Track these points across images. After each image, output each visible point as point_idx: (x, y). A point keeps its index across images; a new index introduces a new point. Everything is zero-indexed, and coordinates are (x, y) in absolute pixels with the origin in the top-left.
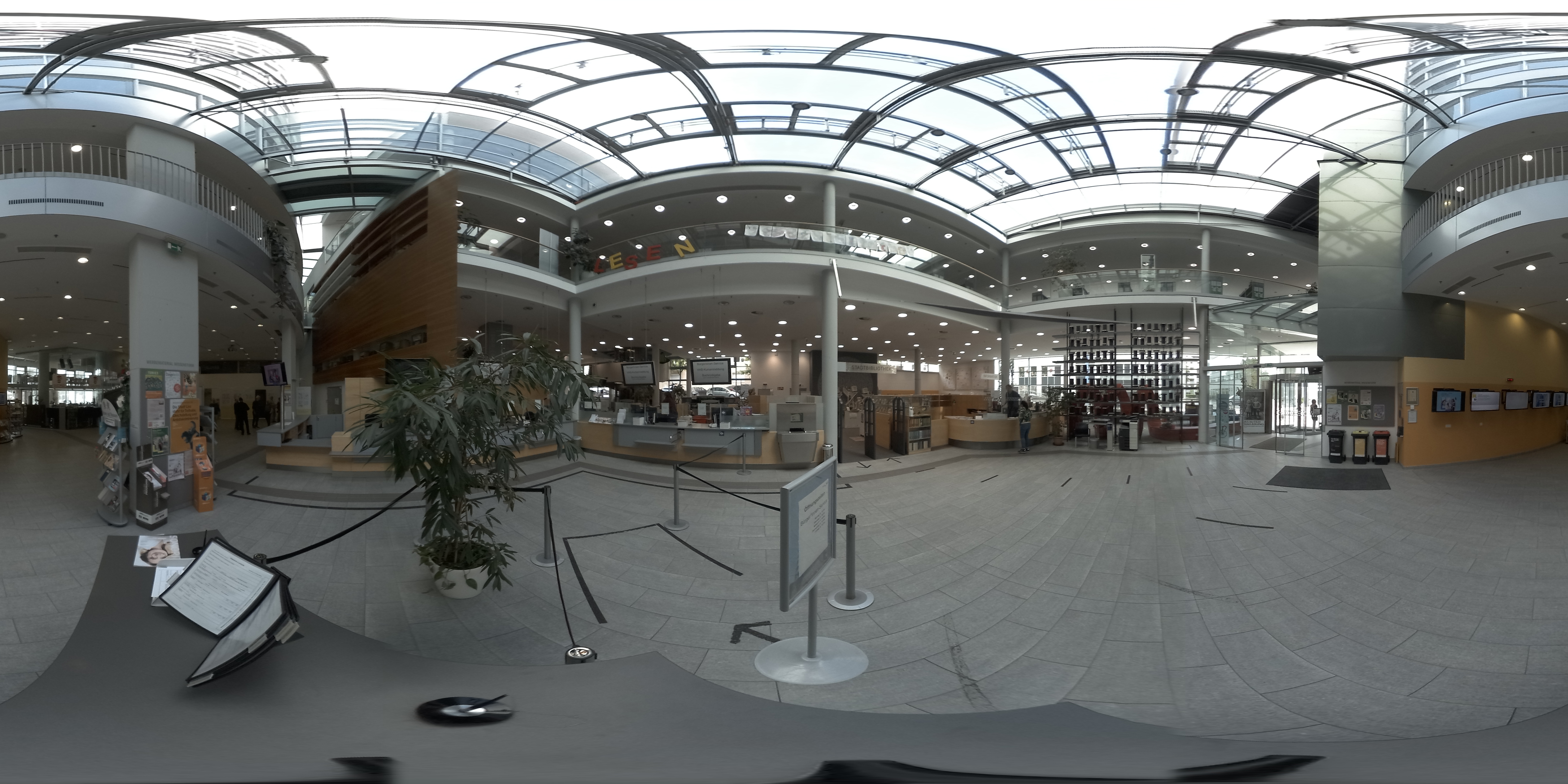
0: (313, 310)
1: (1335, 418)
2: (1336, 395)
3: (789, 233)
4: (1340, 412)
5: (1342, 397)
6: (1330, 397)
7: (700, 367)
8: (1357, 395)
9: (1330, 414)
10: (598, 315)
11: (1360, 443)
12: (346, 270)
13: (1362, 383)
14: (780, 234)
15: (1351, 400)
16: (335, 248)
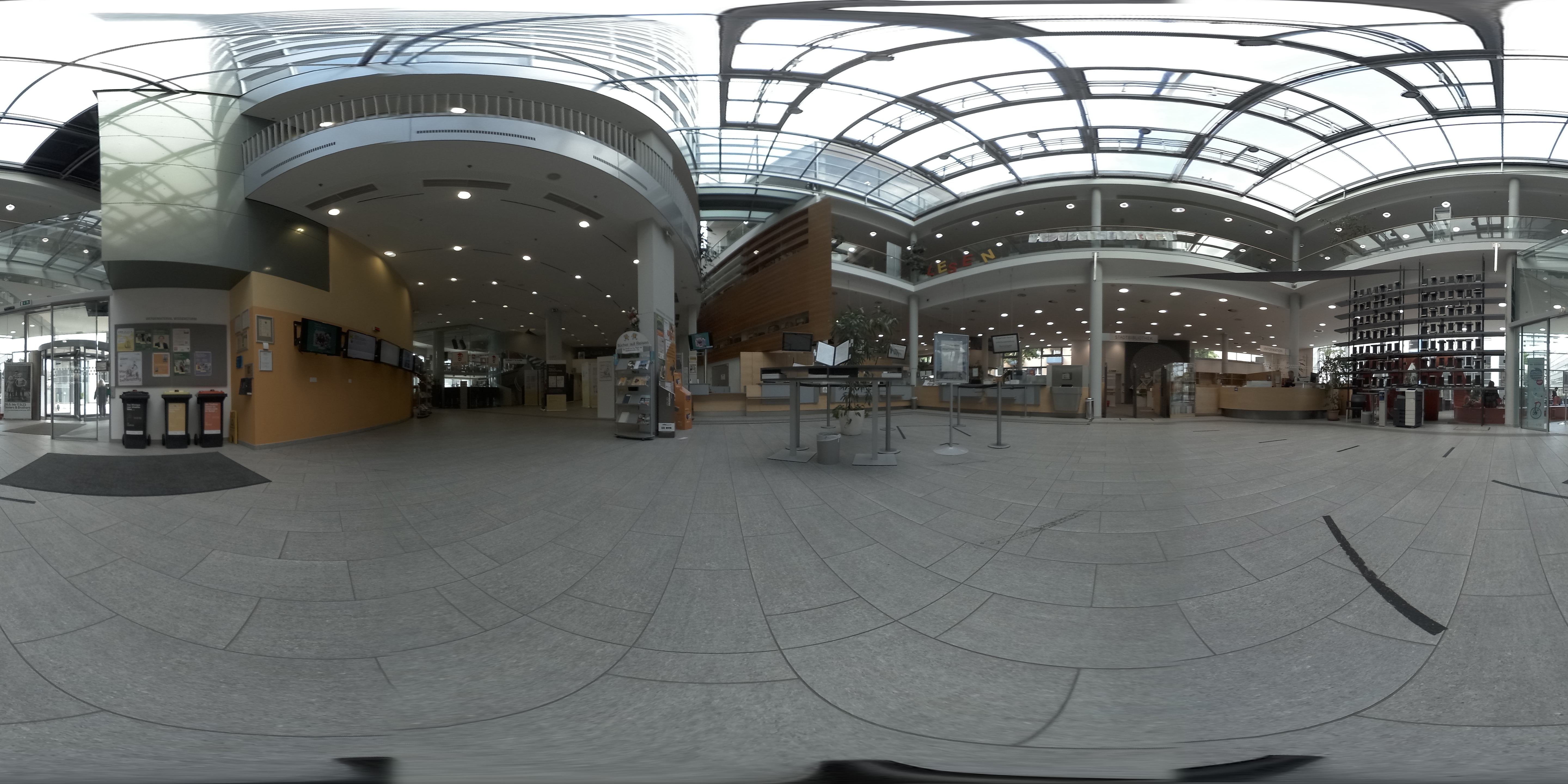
1: (131, 375)
2: (132, 338)
3: (1061, 237)
4: (139, 364)
5: (143, 340)
6: (122, 341)
8: (167, 337)
9: (124, 366)
10: (931, 308)
11: (176, 410)
12: (721, 278)
13: (175, 319)
14: (1054, 238)
15: (158, 345)
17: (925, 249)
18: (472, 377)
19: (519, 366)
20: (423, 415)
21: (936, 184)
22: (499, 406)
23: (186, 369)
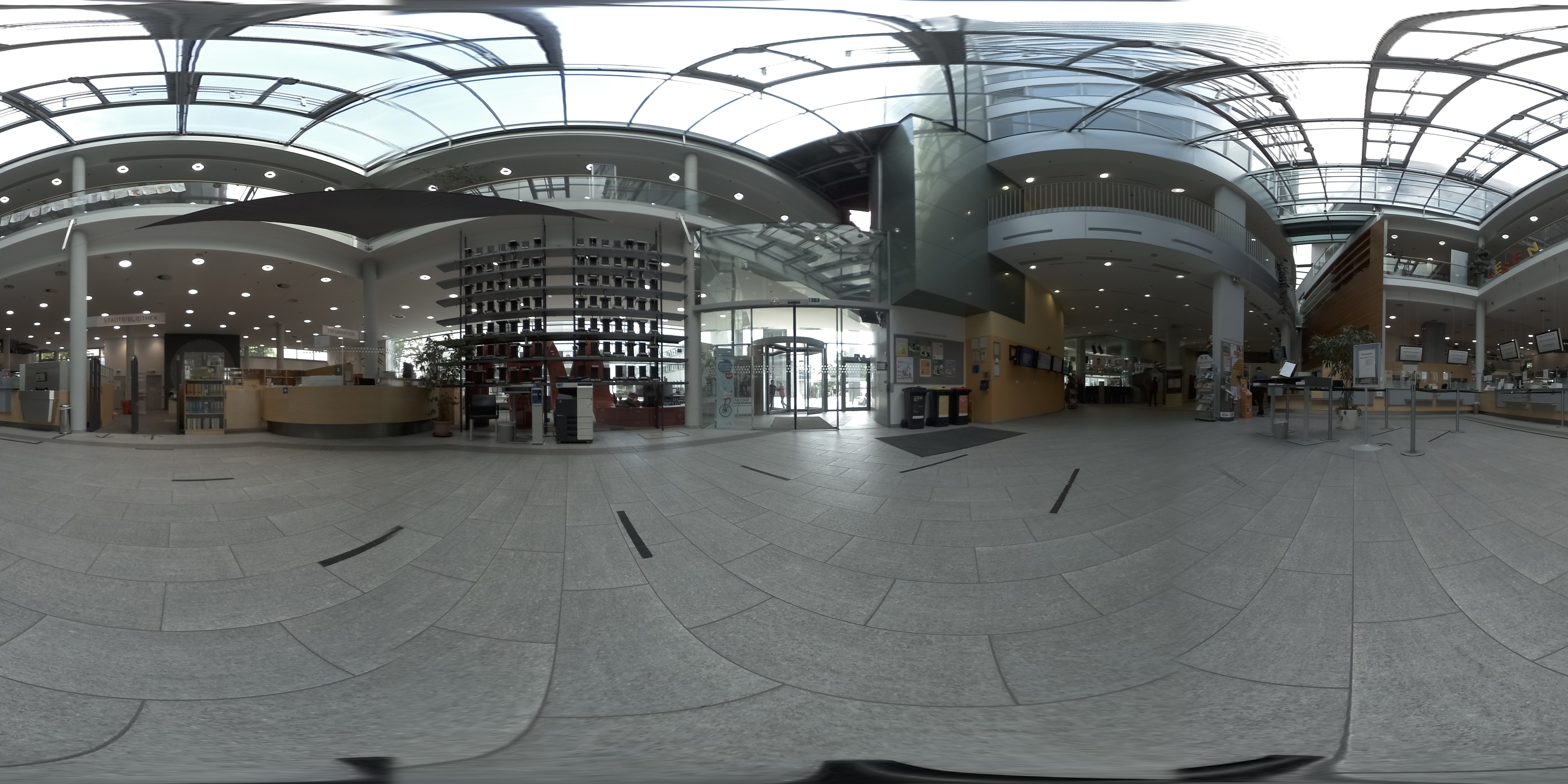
0: (1302, 313)
1: (905, 375)
2: (906, 347)
4: (911, 367)
5: (914, 349)
6: (899, 348)
7: (1405, 350)
8: (929, 348)
15: (923, 353)
16: (1321, 265)
17: (1489, 253)
18: (1108, 377)
19: (1148, 370)
20: (1072, 408)
21: (1479, 186)
22: (1130, 403)
23: (940, 372)
